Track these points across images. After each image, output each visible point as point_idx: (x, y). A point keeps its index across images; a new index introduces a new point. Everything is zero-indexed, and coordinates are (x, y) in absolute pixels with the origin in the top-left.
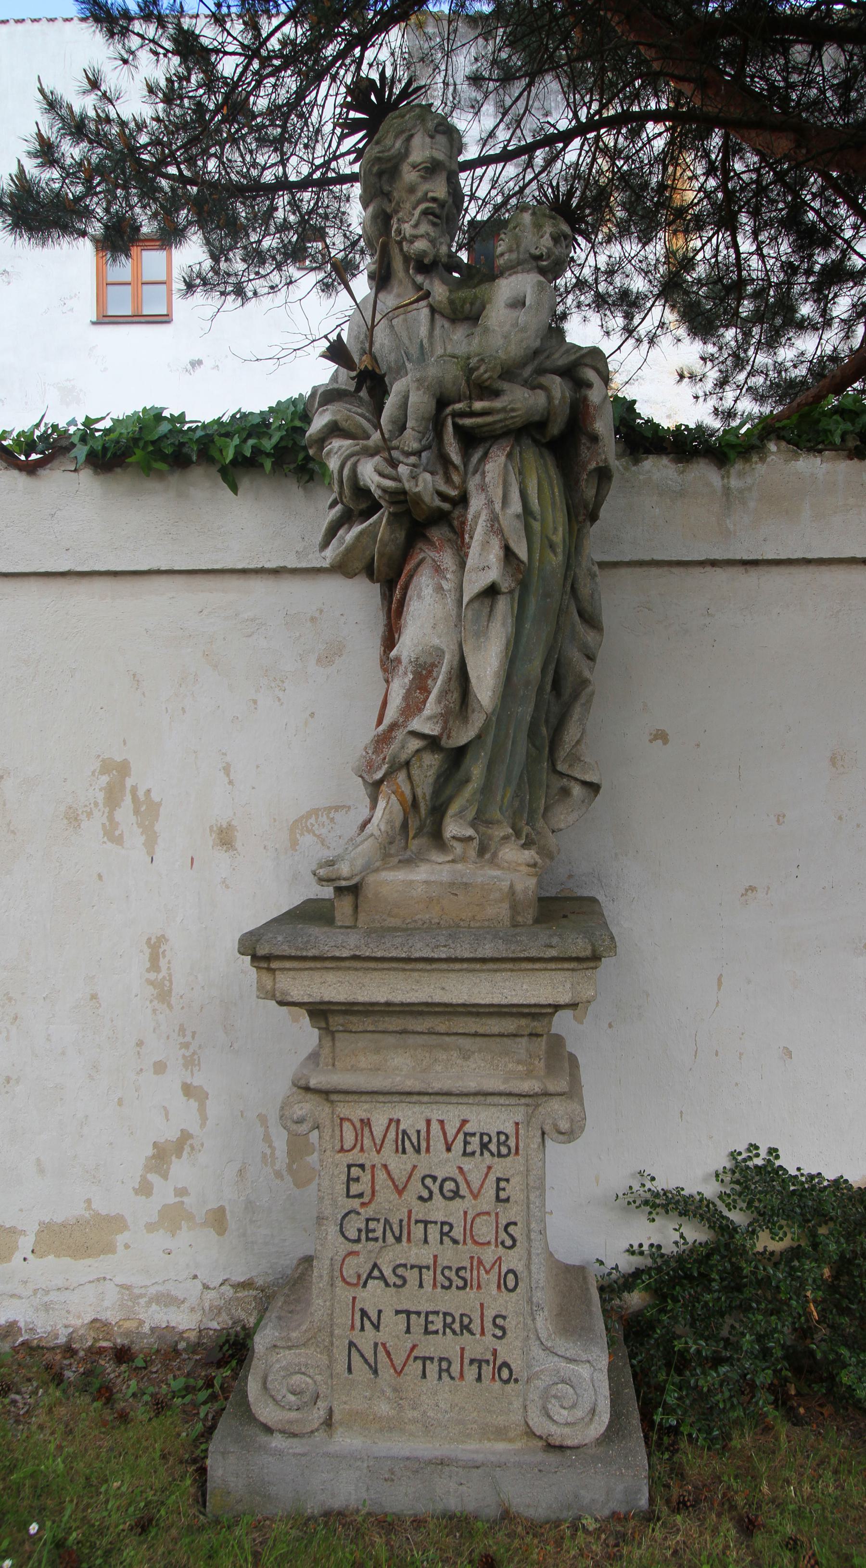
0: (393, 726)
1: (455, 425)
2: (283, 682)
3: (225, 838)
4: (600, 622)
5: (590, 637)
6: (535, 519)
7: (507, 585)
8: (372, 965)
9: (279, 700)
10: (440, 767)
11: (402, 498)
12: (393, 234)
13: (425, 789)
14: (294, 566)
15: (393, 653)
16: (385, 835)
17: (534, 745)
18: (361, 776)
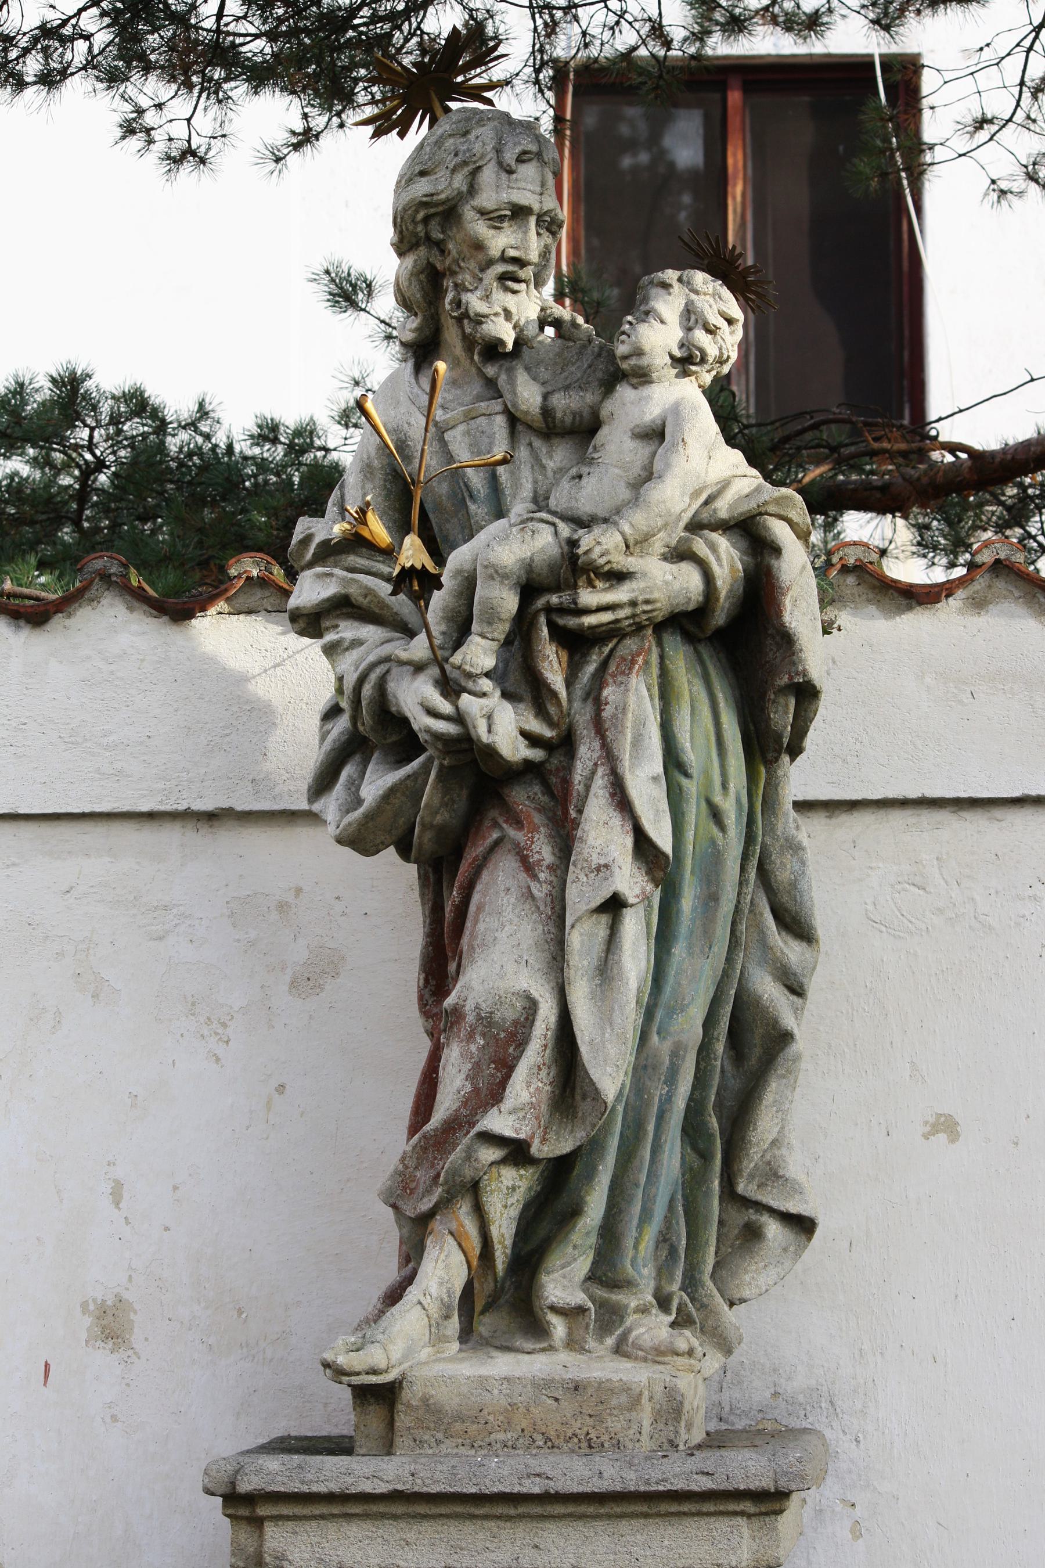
0: (454, 1126)
1: (551, 625)
2: (224, 1025)
3: (111, 1325)
4: (811, 927)
5: (792, 951)
6: (687, 775)
7: (637, 891)
8: (422, 1509)
9: (218, 1060)
10: (530, 1189)
11: (465, 746)
12: (447, 307)
13: (503, 1226)
14: (247, 807)
15: (449, 1001)
16: (438, 1303)
17: (695, 1148)
18: (394, 1206)
